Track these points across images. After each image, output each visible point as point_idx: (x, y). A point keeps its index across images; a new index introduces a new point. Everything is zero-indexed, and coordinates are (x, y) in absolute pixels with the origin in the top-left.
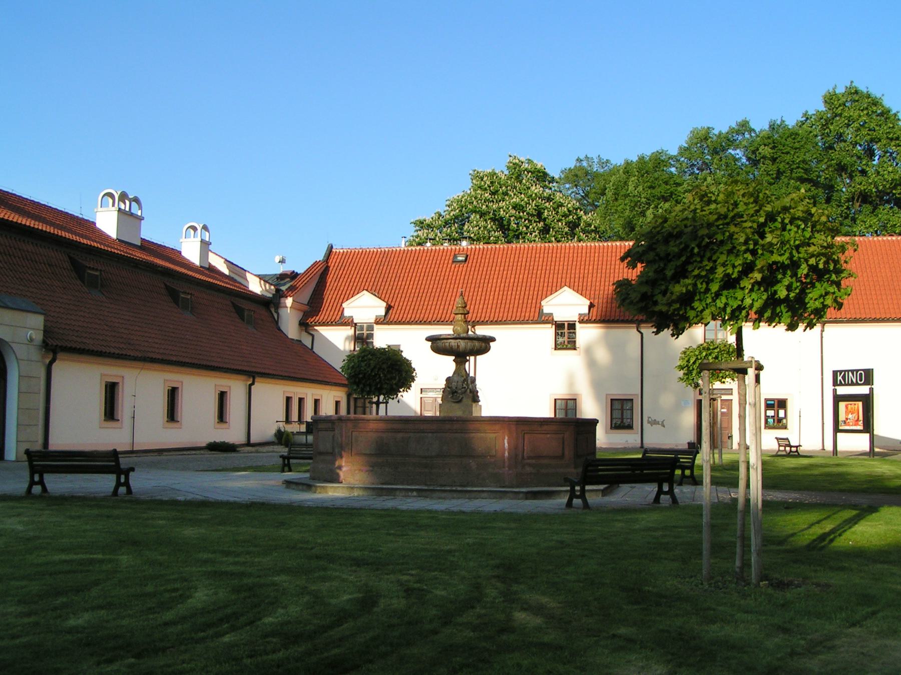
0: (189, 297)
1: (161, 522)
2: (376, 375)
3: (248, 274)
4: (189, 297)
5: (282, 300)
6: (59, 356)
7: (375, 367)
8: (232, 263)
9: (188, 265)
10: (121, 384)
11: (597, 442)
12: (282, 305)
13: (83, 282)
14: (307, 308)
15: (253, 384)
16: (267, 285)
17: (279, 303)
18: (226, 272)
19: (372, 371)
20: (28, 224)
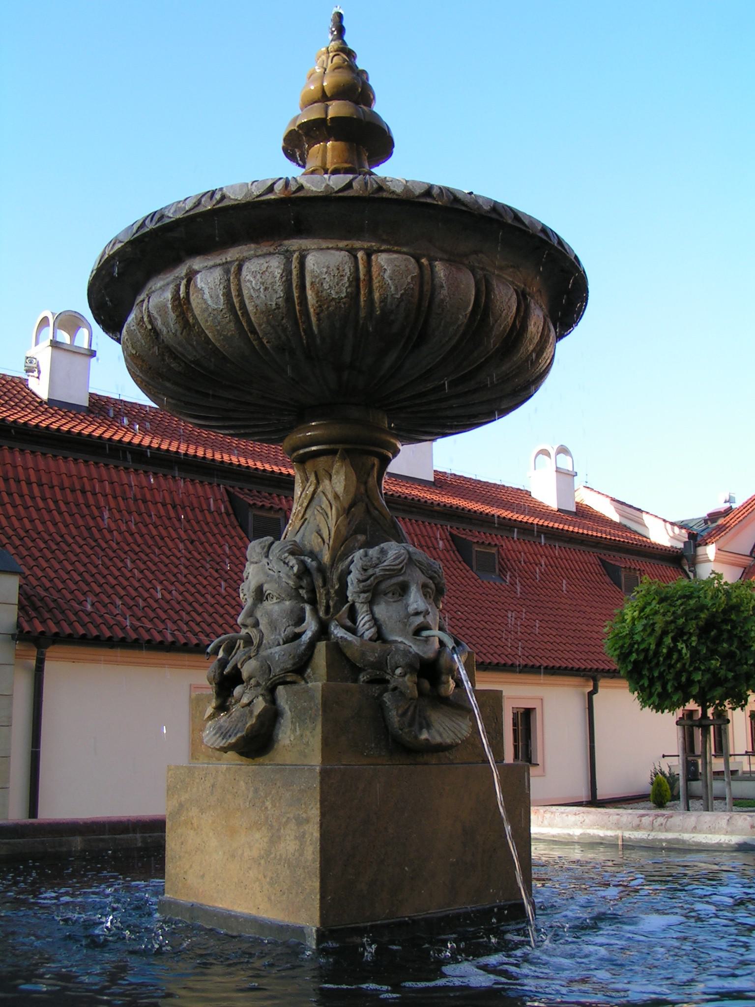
0: (494, 550)
1: (105, 998)
2: (671, 651)
3: (644, 516)
4: (494, 550)
5: (700, 550)
6: (602, 683)
7: (665, 633)
8: (618, 501)
9: (539, 510)
10: (538, 711)
11: (532, 854)
12: (701, 558)
13: (469, 564)
14: (749, 561)
15: (595, 691)
16: (677, 530)
17: (695, 556)
18: (616, 518)
19: (659, 643)
20: (173, 449)
